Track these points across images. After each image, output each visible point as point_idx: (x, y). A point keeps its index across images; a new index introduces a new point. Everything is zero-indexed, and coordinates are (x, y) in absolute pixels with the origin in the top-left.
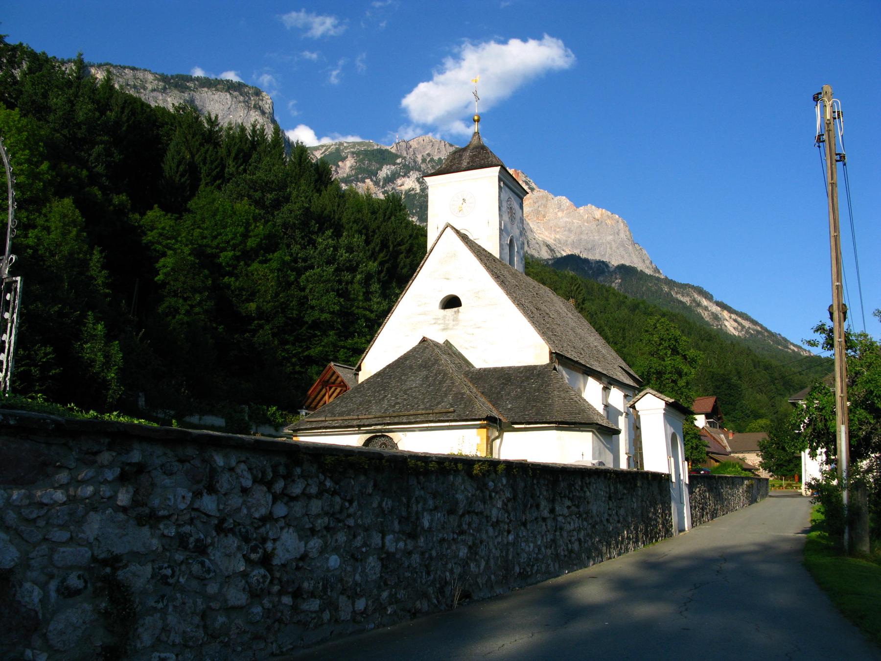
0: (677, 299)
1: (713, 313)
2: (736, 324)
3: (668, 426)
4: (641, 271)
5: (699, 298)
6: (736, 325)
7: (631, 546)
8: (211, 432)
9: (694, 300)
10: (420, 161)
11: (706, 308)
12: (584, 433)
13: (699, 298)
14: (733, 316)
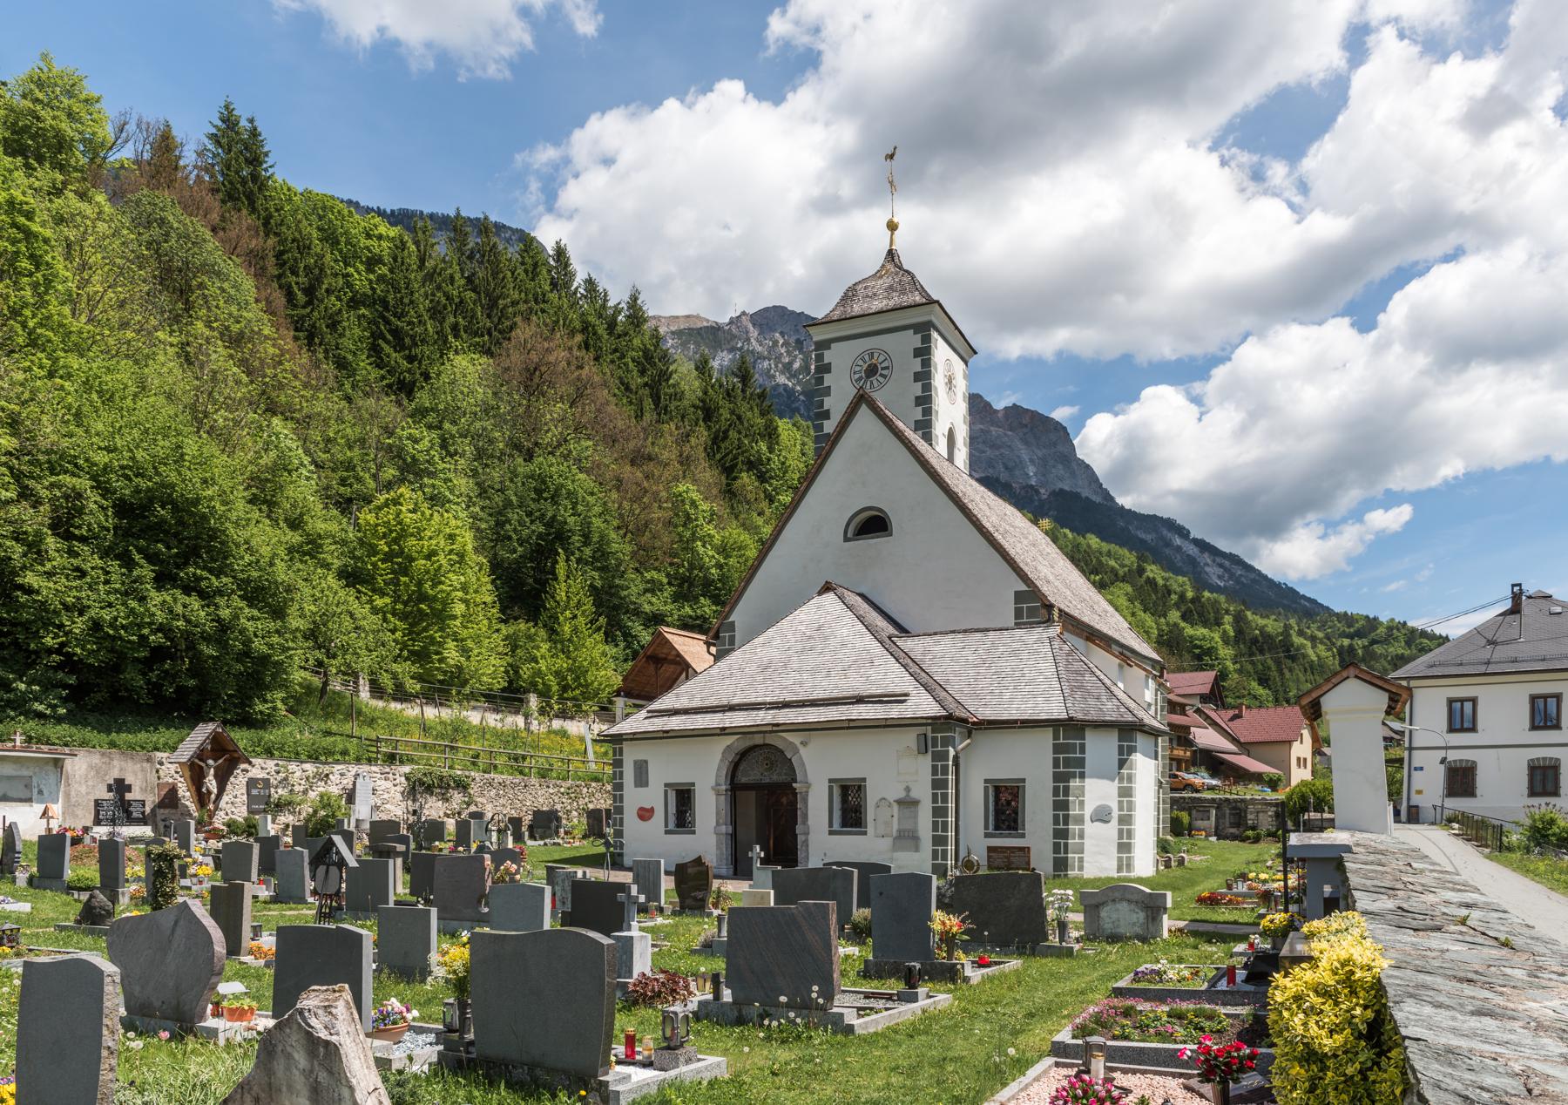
3: (1097, 499)
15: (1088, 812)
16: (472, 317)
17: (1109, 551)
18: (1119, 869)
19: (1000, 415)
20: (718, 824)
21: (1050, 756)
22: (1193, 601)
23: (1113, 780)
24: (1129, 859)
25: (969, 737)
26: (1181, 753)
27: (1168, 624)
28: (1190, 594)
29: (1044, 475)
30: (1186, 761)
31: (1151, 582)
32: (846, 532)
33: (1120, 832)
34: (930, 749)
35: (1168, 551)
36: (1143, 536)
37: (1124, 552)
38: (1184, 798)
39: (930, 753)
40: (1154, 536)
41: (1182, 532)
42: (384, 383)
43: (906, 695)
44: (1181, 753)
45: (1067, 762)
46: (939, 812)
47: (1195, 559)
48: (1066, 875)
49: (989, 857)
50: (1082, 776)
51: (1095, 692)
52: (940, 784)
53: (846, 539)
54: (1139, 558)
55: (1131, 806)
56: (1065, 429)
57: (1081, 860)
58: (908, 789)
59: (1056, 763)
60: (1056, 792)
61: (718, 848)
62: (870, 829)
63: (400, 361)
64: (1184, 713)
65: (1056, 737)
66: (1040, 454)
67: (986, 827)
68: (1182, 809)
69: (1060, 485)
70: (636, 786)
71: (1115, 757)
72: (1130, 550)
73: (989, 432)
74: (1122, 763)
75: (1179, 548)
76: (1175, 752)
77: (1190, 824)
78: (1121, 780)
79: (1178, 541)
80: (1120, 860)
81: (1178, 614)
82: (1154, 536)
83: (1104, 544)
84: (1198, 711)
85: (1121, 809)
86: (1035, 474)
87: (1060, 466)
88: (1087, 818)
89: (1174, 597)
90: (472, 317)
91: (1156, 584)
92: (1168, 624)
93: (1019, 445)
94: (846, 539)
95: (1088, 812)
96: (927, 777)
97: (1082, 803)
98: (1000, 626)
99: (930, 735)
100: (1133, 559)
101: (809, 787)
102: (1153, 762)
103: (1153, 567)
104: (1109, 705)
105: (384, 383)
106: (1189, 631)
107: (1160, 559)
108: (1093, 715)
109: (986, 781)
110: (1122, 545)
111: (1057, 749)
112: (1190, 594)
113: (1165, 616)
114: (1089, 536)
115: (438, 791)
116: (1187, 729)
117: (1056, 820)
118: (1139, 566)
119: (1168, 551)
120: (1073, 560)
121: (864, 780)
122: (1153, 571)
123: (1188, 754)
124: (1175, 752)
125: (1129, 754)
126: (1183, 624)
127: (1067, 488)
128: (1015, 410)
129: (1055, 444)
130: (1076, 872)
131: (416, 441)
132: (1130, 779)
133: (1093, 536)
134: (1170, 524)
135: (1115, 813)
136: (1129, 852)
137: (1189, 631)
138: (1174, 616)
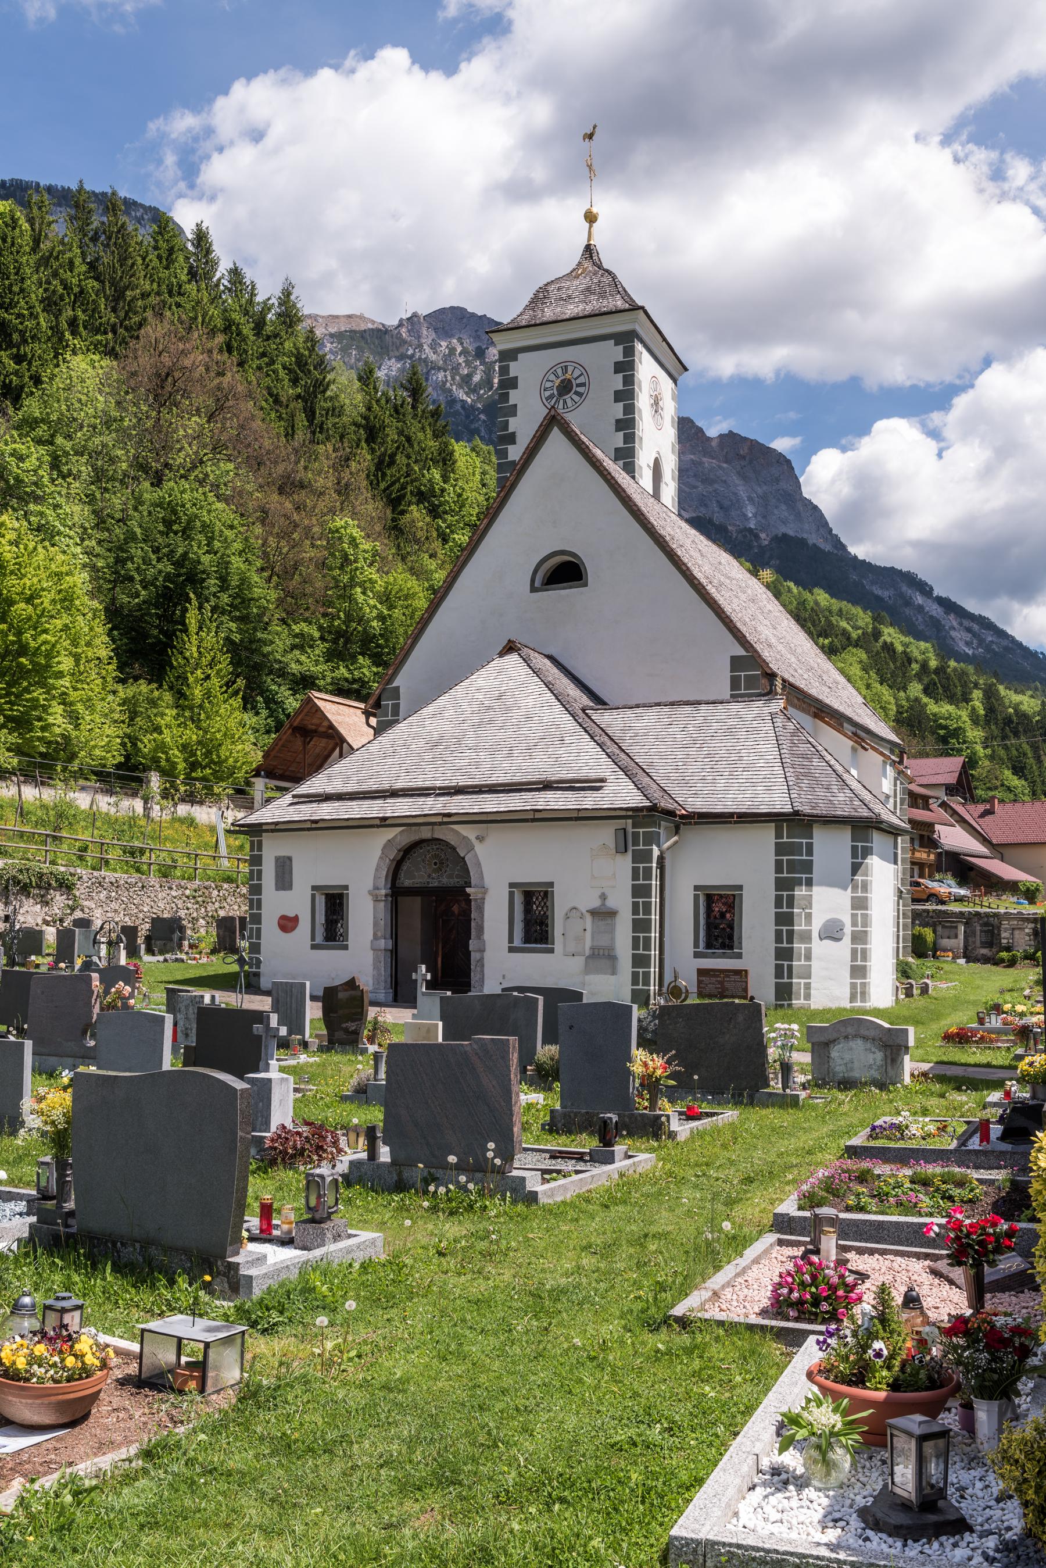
0: (873, 594)
1: (931, 617)
2: (970, 635)
3: (827, 547)
4: (814, 545)
5: (909, 592)
6: (968, 637)
7: (335, 1266)
8: (937, 1252)
9: (901, 595)
10: (899, 1300)
11: (920, 608)
12: (456, 585)
13: (909, 592)
14: (966, 623)
16: (94, 311)
17: (840, 610)
18: (853, 998)
19: (714, 444)
20: (376, 937)
22: (937, 671)
23: (845, 889)
24: (864, 985)
25: (677, 833)
26: (924, 856)
27: (908, 699)
28: (933, 663)
29: (764, 517)
31: (889, 648)
32: (533, 581)
33: (854, 952)
34: (631, 848)
36: (878, 592)
37: (857, 611)
38: (927, 911)
39: (630, 853)
40: (892, 592)
41: (924, 589)
44: (924, 856)
45: (792, 867)
47: (938, 621)
48: (790, 1005)
49: (699, 982)
50: (809, 883)
55: (866, 921)
57: (808, 986)
58: (603, 897)
59: (779, 868)
61: (376, 967)
62: (558, 946)
64: (926, 807)
65: (779, 835)
66: (760, 491)
68: (925, 925)
72: (865, 609)
73: (701, 463)
74: (855, 868)
76: (917, 855)
77: (935, 943)
78: (855, 888)
80: (853, 986)
81: (920, 687)
82: (892, 592)
83: (834, 601)
85: (854, 924)
86: (755, 515)
87: (784, 507)
88: (815, 935)
89: (915, 666)
90: (94, 311)
91: (894, 651)
92: (908, 699)
93: (737, 480)
97: (809, 916)
102: (893, 866)
103: (891, 630)
106: (933, 707)
108: (822, 809)
109: (697, 888)
110: (854, 603)
112: (933, 663)
113: (905, 689)
114: (816, 590)
116: (930, 826)
117: (778, 938)
118: (874, 628)
122: (890, 634)
123: (932, 857)
125: (864, 857)
126: (925, 700)
127: (791, 533)
128: (731, 439)
130: (802, 1001)
132: (865, 887)
134: (910, 579)
135: (848, 929)
136: (864, 977)
137: (933, 707)
138: (915, 689)
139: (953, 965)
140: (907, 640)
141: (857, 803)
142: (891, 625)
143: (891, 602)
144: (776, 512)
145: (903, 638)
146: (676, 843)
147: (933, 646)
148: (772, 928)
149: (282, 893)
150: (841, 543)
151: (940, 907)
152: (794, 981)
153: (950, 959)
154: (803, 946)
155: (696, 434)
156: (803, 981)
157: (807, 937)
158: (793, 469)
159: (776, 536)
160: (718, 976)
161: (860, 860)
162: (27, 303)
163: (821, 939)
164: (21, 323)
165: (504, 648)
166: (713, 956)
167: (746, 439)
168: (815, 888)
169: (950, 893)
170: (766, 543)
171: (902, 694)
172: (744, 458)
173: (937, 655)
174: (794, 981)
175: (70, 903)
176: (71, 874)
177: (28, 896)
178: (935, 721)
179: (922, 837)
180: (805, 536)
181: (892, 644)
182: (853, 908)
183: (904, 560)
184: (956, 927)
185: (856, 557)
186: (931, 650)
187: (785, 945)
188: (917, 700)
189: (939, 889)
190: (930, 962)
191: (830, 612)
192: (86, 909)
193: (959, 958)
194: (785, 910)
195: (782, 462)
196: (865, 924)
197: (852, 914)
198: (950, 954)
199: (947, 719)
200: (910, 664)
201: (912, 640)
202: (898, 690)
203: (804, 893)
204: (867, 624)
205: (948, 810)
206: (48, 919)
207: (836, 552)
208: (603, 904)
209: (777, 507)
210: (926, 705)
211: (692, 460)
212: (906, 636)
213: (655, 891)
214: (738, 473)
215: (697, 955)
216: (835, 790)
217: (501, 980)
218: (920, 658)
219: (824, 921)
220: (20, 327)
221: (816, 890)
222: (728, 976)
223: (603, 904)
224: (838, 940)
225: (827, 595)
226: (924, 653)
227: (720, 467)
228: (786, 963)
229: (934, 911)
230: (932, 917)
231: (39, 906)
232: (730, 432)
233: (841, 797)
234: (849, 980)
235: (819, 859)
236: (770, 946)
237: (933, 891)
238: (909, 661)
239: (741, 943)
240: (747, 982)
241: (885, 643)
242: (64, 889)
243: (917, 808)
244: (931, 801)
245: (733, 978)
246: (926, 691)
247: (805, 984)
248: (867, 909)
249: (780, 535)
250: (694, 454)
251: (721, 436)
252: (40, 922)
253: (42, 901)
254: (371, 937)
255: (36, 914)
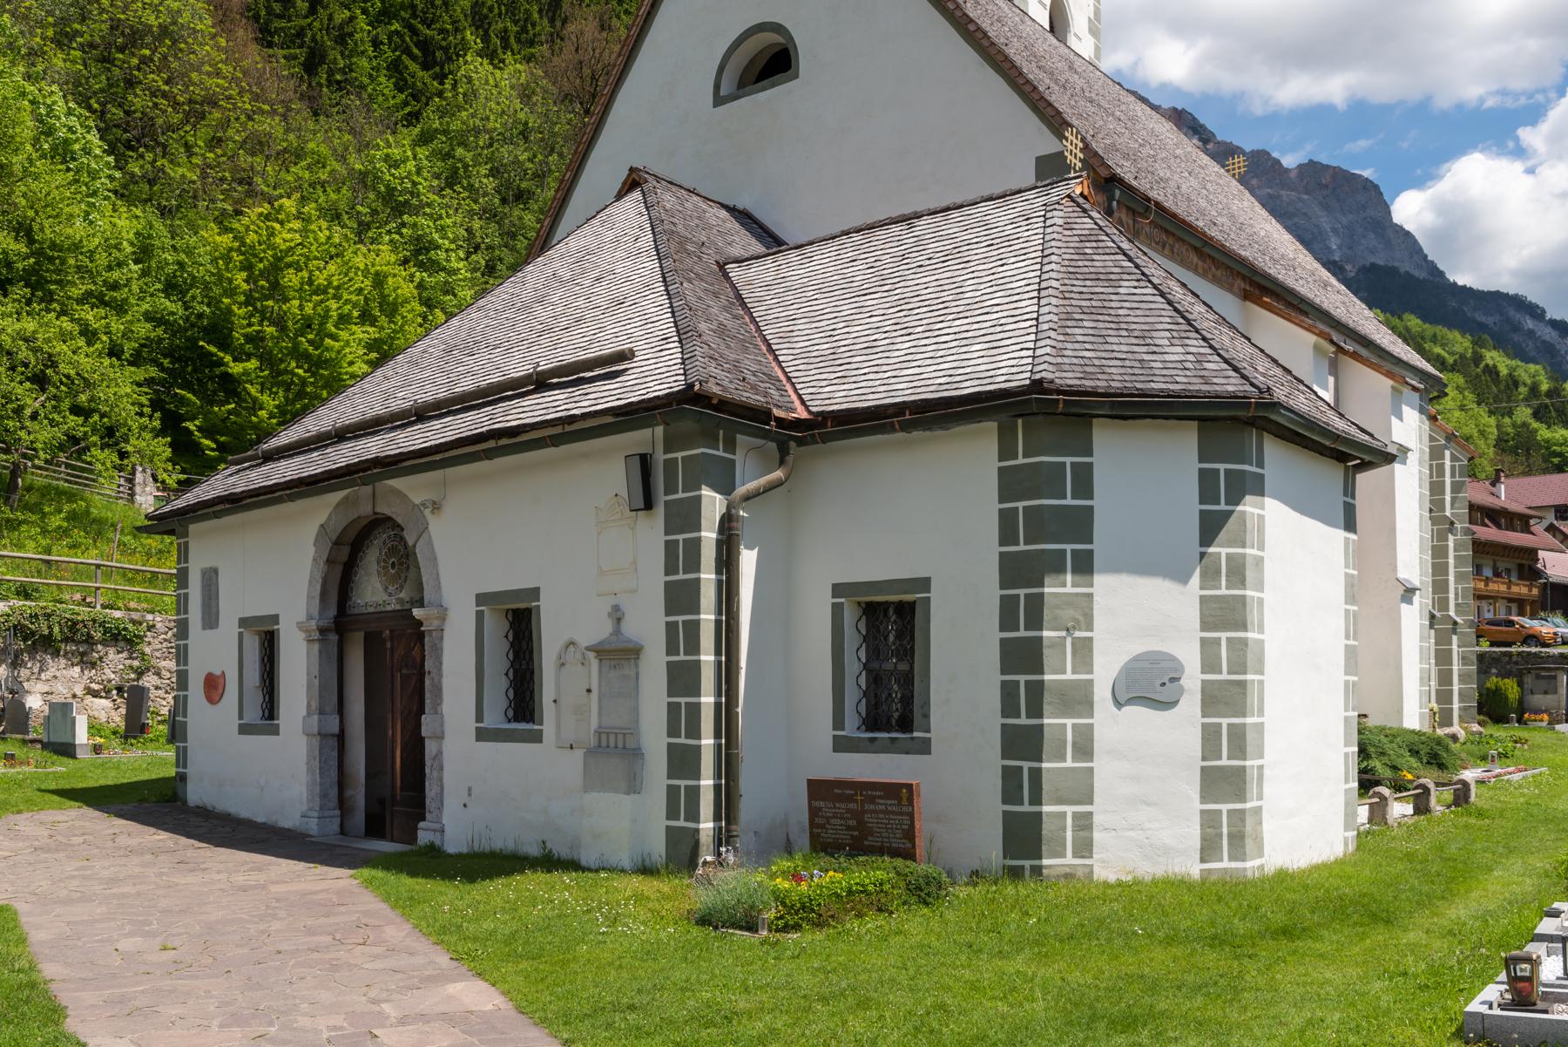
1: (1544, 342)
3: (1420, 274)
4: (1407, 273)
11: (1531, 333)
15: (1105, 672)
16: (526, 20)
17: (1435, 336)
18: (1209, 849)
19: (1293, 175)
20: (309, 714)
21: (989, 506)
22: (1549, 394)
23: (1184, 579)
24: (1238, 817)
25: (782, 462)
26: (1524, 590)
27: (1514, 425)
28: (1545, 387)
29: (1350, 248)
30: (1533, 603)
31: (1492, 371)
32: (717, 87)
33: (1210, 737)
34: (661, 498)
35: (1516, 337)
36: (1483, 319)
37: (1455, 335)
38: (1510, 654)
39: (660, 511)
40: (1497, 318)
41: (1535, 312)
42: (408, 109)
43: (624, 356)
44: (1524, 590)
45: (1040, 525)
46: (683, 679)
47: (1552, 345)
48: (1037, 871)
49: (814, 812)
50: (1085, 566)
51: (1138, 321)
52: (681, 598)
53: (719, 101)
54: (1474, 343)
55: (1242, 657)
56: (1376, 187)
57: (1084, 823)
58: (617, 616)
59: (1007, 533)
60: (1008, 616)
61: (310, 770)
62: (548, 727)
63: (428, 80)
64: (1526, 529)
65: (1006, 451)
66: (1345, 221)
67: (838, 723)
68: (1504, 675)
69: (1373, 259)
70: (204, 628)
71: (1191, 507)
72: (1463, 333)
73: (1279, 197)
74: (1211, 528)
75: (1531, 333)
76: (1515, 589)
77: (1521, 701)
78: (1210, 577)
79: (1530, 324)
80: (1209, 821)
81: (1529, 411)
82: (1497, 318)
83: (1427, 326)
84: (1551, 529)
85: (1209, 664)
86: (1340, 247)
87: (1372, 236)
88: (1102, 693)
89: (1522, 389)
90: (526, 20)
91: (1497, 374)
92: (1514, 425)
93: (1318, 211)
94: (719, 101)
95: (1105, 672)
96: (654, 580)
97: (1084, 651)
98: (944, 204)
99: (660, 457)
100: (1467, 344)
101: (443, 619)
102: (1341, 534)
103: (1494, 354)
104: (1175, 354)
105: (408, 109)
106: (1544, 433)
107: (1500, 343)
108: (1115, 378)
109: (838, 590)
110: (1451, 326)
111: (1011, 484)
112: (1545, 387)
113: (1510, 414)
114: (1407, 316)
115: (71, 647)
116: (1532, 553)
117: (1009, 704)
118: (1475, 352)
119: (1516, 337)
120: (1272, 212)
121: (535, 593)
122: (1492, 357)
123: (1535, 591)
124: (1515, 589)
125: (1235, 498)
126: (1535, 425)
127: (1381, 263)
128: (1311, 169)
129: (1364, 208)
130: (1069, 859)
131: (396, 165)
132: (1238, 572)
133: (1412, 317)
134: (1518, 302)
135: (1193, 679)
136: (1241, 796)
137: (1544, 433)
138: (1523, 414)
139: (1549, 734)
140: (1514, 363)
141: (1214, 365)
142: (1495, 349)
143: (1496, 329)
144: (1363, 241)
145: (1509, 362)
146: (778, 484)
147: (1544, 368)
148: (993, 677)
149: (209, 632)
150: (1438, 269)
151: (1543, 650)
152: (1046, 809)
153: (1544, 724)
154: (1069, 722)
155: (1273, 166)
156: (1069, 810)
157: (1079, 698)
158: (1382, 194)
159: (1364, 267)
160: (850, 799)
161: (1223, 507)
162: (450, 17)
163: (1119, 704)
164: (444, 39)
165: (624, 183)
166: (871, 746)
167: (1328, 166)
168: (1098, 579)
169: (1555, 634)
170: (1353, 274)
171: (1507, 420)
172: (1326, 186)
173: (1549, 378)
174: (1046, 809)
175: (136, 663)
176: (134, 622)
177: (56, 654)
178: (1548, 448)
179: (1521, 567)
180: (1396, 264)
181: (1495, 367)
182: (1205, 626)
183: (1508, 285)
184: (1555, 677)
185: (1455, 284)
186: (1543, 372)
187: (1023, 720)
188: (1524, 425)
189: (1539, 628)
190: (1515, 730)
191: (1423, 338)
192: (164, 672)
193: (1559, 722)
194: (1022, 633)
195: (1370, 188)
196: (1239, 666)
197: (1204, 642)
198: (1546, 717)
199: (1562, 445)
200: (1517, 388)
201: (1519, 363)
202: (1503, 416)
203: (1069, 589)
204: (1465, 349)
205: (1557, 534)
206: (95, 687)
207: (1431, 279)
208: (617, 631)
209: (1364, 237)
210: (1536, 431)
211: (1269, 194)
212: (1512, 359)
213: (708, 596)
214: (1321, 203)
215: (841, 745)
216: (1162, 339)
217: (466, 799)
218: (1529, 381)
219: (1125, 658)
220: (444, 43)
221: (1103, 584)
222: (872, 800)
223: (617, 631)
224: (1168, 705)
225: (1419, 321)
226: (1534, 377)
227: (1299, 199)
228: (1026, 765)
229: (1519, 654)
230: (1516, 663)
231: (77, 669)
232: (1311, 161)
233: (1175, 354)
234: (1198, 806)
235: (1106, 504)
236: (990, 721)
237: (1531, 632)
238: (1516, 384)
239: (927, 716)
240: (911, 815)
241: (1487, 365)
242: (122, 644)
243: (1513, 530)
244: (1532, 522)
245: (882, 804)
246: (1536, 415)
247: (1076, 816)
248: (1244, 627)
249: (1368, 265)
250: (1271, 188)
251: (1300, 166)
252: (79, 690)
253: (82, 661)
254: (304, 712)
255: (72, 680)
